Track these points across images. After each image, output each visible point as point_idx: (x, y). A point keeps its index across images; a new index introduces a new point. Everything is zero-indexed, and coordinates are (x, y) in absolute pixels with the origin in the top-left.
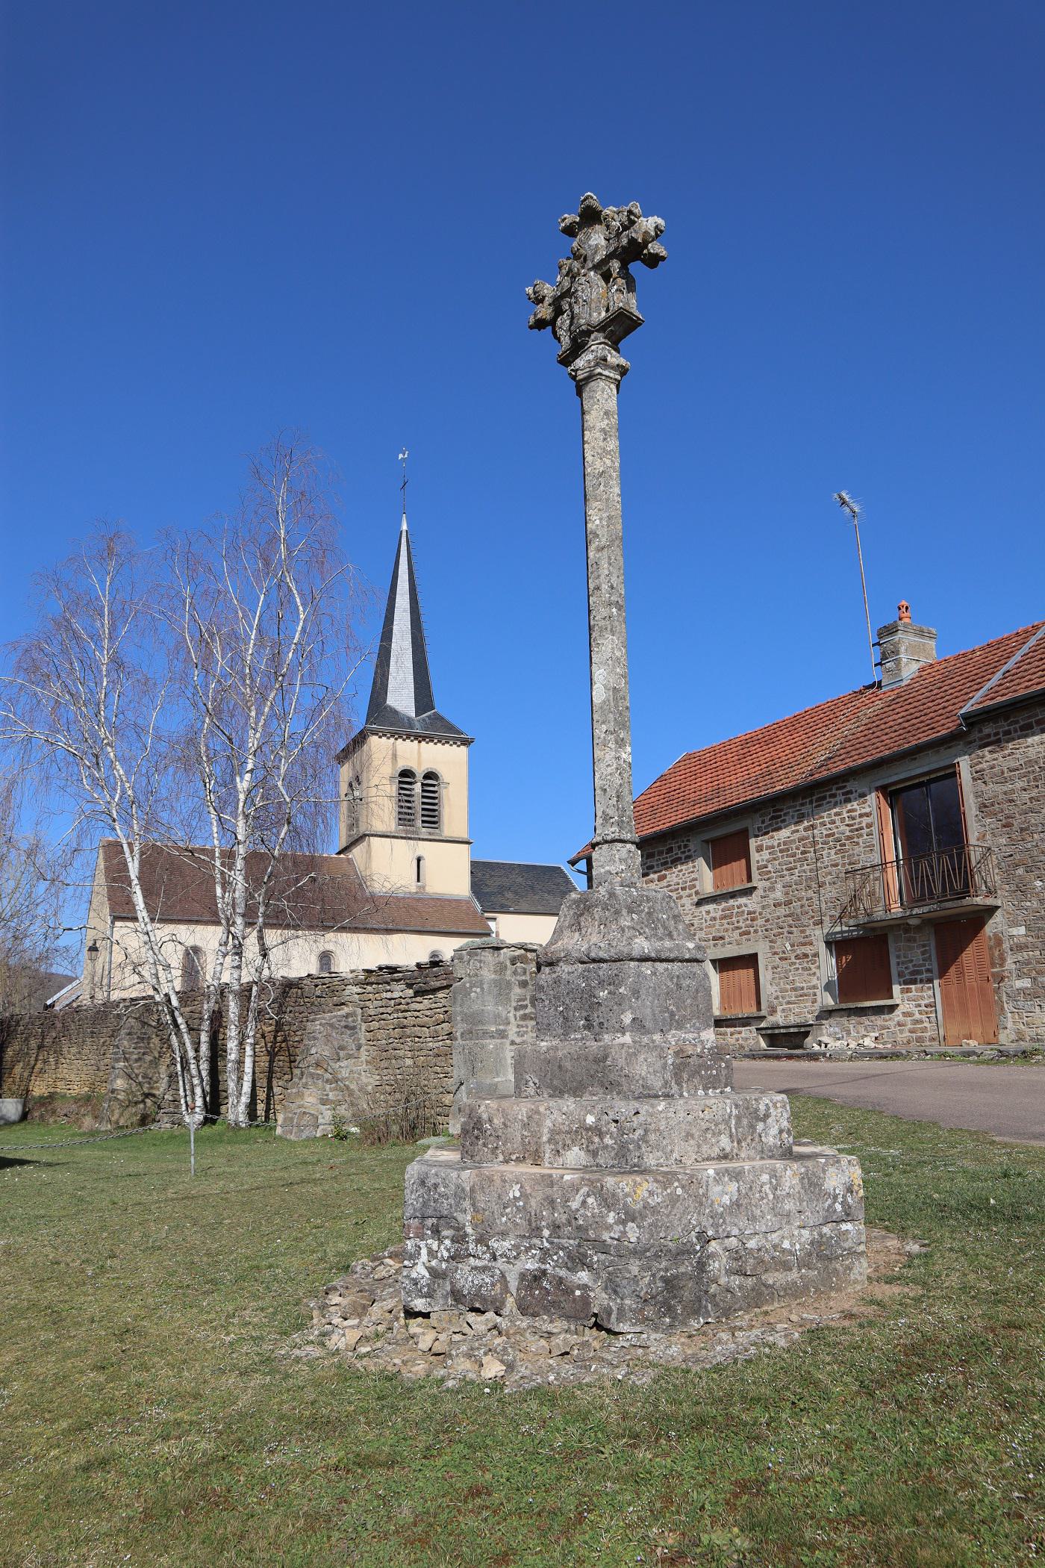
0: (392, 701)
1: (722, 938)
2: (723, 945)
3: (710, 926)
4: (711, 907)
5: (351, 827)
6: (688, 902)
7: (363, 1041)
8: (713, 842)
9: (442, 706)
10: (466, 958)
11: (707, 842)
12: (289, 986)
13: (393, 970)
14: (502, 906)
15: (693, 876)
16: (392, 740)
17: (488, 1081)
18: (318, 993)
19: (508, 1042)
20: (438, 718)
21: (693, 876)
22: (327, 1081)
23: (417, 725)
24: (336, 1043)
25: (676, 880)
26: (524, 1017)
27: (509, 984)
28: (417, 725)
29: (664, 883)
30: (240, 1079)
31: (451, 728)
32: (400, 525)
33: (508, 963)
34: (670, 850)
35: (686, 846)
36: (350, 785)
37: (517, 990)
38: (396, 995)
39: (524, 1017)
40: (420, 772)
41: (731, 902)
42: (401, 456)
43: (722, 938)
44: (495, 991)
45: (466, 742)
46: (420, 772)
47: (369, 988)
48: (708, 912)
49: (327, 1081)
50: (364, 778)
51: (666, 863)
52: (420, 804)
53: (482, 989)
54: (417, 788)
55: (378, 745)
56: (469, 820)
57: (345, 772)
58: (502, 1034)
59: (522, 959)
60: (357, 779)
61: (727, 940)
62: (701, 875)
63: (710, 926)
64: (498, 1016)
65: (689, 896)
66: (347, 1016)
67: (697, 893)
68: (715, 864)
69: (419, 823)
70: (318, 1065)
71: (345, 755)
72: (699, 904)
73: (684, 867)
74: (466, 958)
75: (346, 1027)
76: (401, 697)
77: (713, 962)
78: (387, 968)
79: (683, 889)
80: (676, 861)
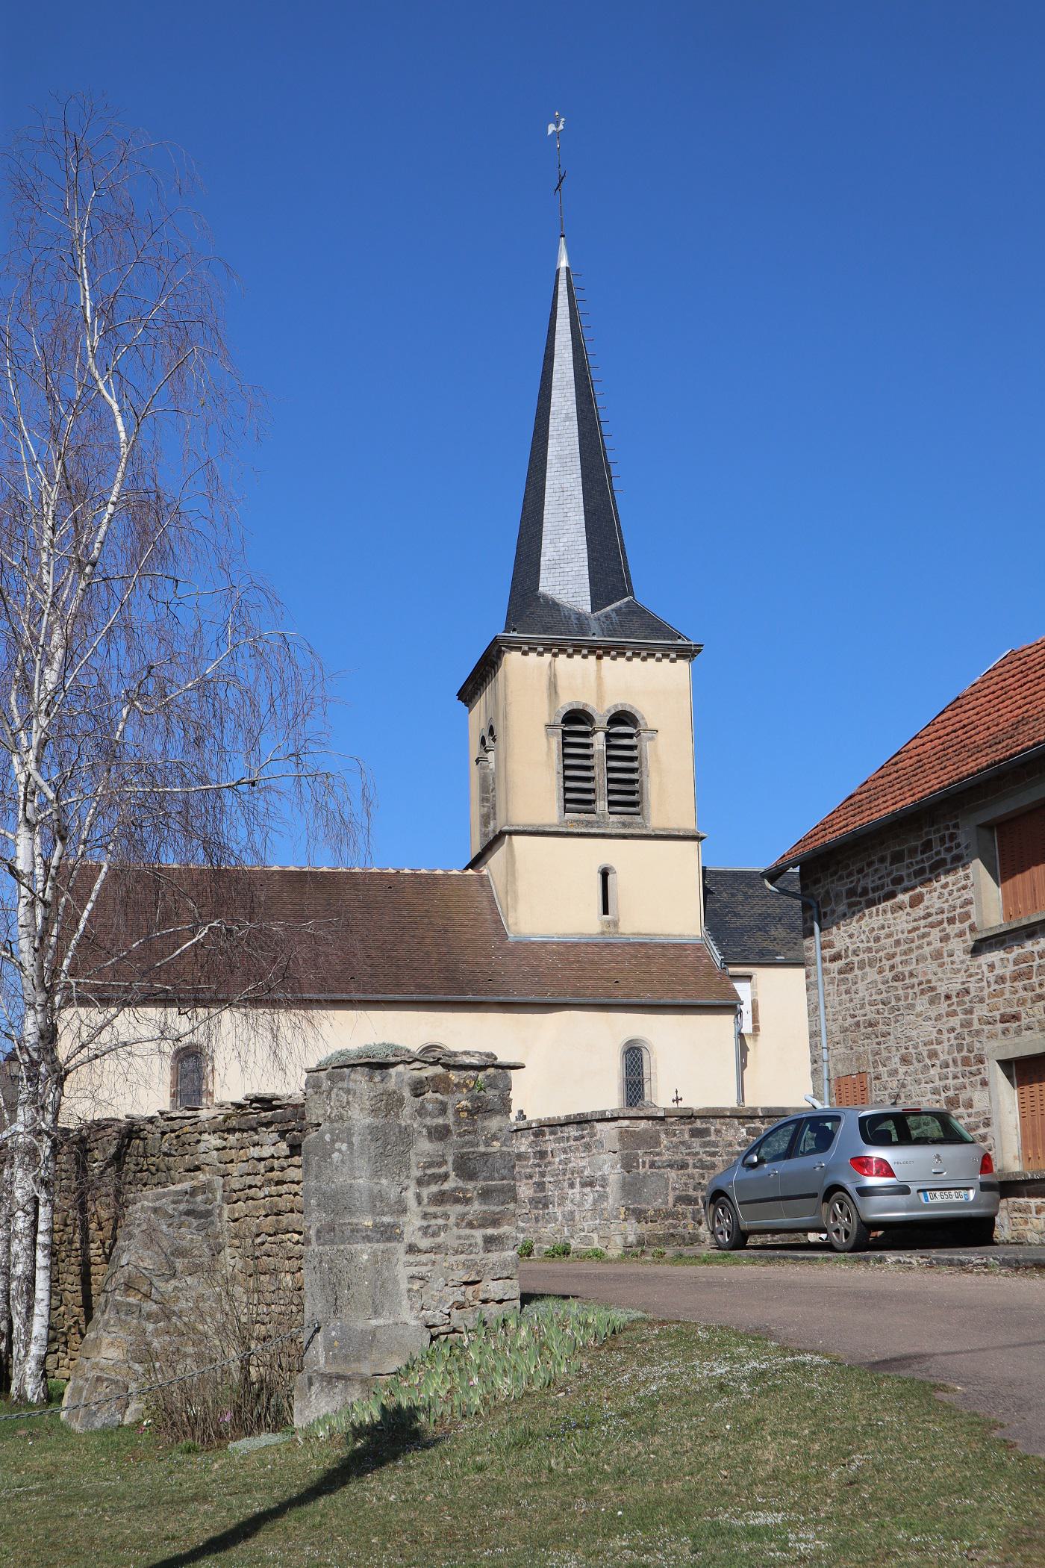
0: (548, 585)
1: (1015, 1017)
2: (1018, 1032)
3: (996, 994)
4: (995, 956)
5: (486, 819)
6: (959, 947)
7: (225, 1239)
8: (1000, 826)
9: (650, 589)
10: (326, 1084)
11: (988, 827)
12: (131, 1131)
13: (265, 1103)
14: (762, 953)
15: (967, 895)
16: (548, 656)
17: (360, 1325)
18: (165, 1148)
19: (401, 1248)
20: (636, 611)
21: (967, 895)
22: (149, 1316)
23: (595, 626)
24: (165, 1243)
25: (938, 904)
26: (440, 1198)
27: (405, 1134)
28: (595, 626)
29: (920, 911)
30: (30, 1309)
31: (659, 628)
32: (555, 259)
33: (407, 1093)
34: (927, 846)
35: (952, 837)
36: (483, 741)
37: (425, 1145)
38: (267, 1151)
39: (440, 1198)
40: (601, 714)
41: (1029, 946)
42: (551, 128)
43: (1015, 1017)
44: (373, 1149)
45: (687, 653)
46: (601, 714)
47: (232, 1139)
48: (991, 967)
49: (149, 1316)
50: (499, 731)
51: (922, 871)
52: (603, 771)
53: (351, 1144)
54: (599, 741)
55: (522, 670)
56: (698, 797)
57: (476, 718)
58: (388, 1233)
59: (439, 1085)
60: (491, 730)
61: (1024, 1022)
62: (978, 894)
63: (996, 994)
64: (381, 1197)
65: (961, 934)
66: (193, 1192)
67: (972, 928)
68: (1004, 870)
69: (602, 806)
70: (129, 1287)
71: (469, 693)
72: (977, 949)
73: (950, 878)
74: (326, 1084)
75: (189, 1213)
76: (565, 575)
77: (1005, 1064)
78: (258, 1100)
79: (951, 921)
80: (939, 868)
